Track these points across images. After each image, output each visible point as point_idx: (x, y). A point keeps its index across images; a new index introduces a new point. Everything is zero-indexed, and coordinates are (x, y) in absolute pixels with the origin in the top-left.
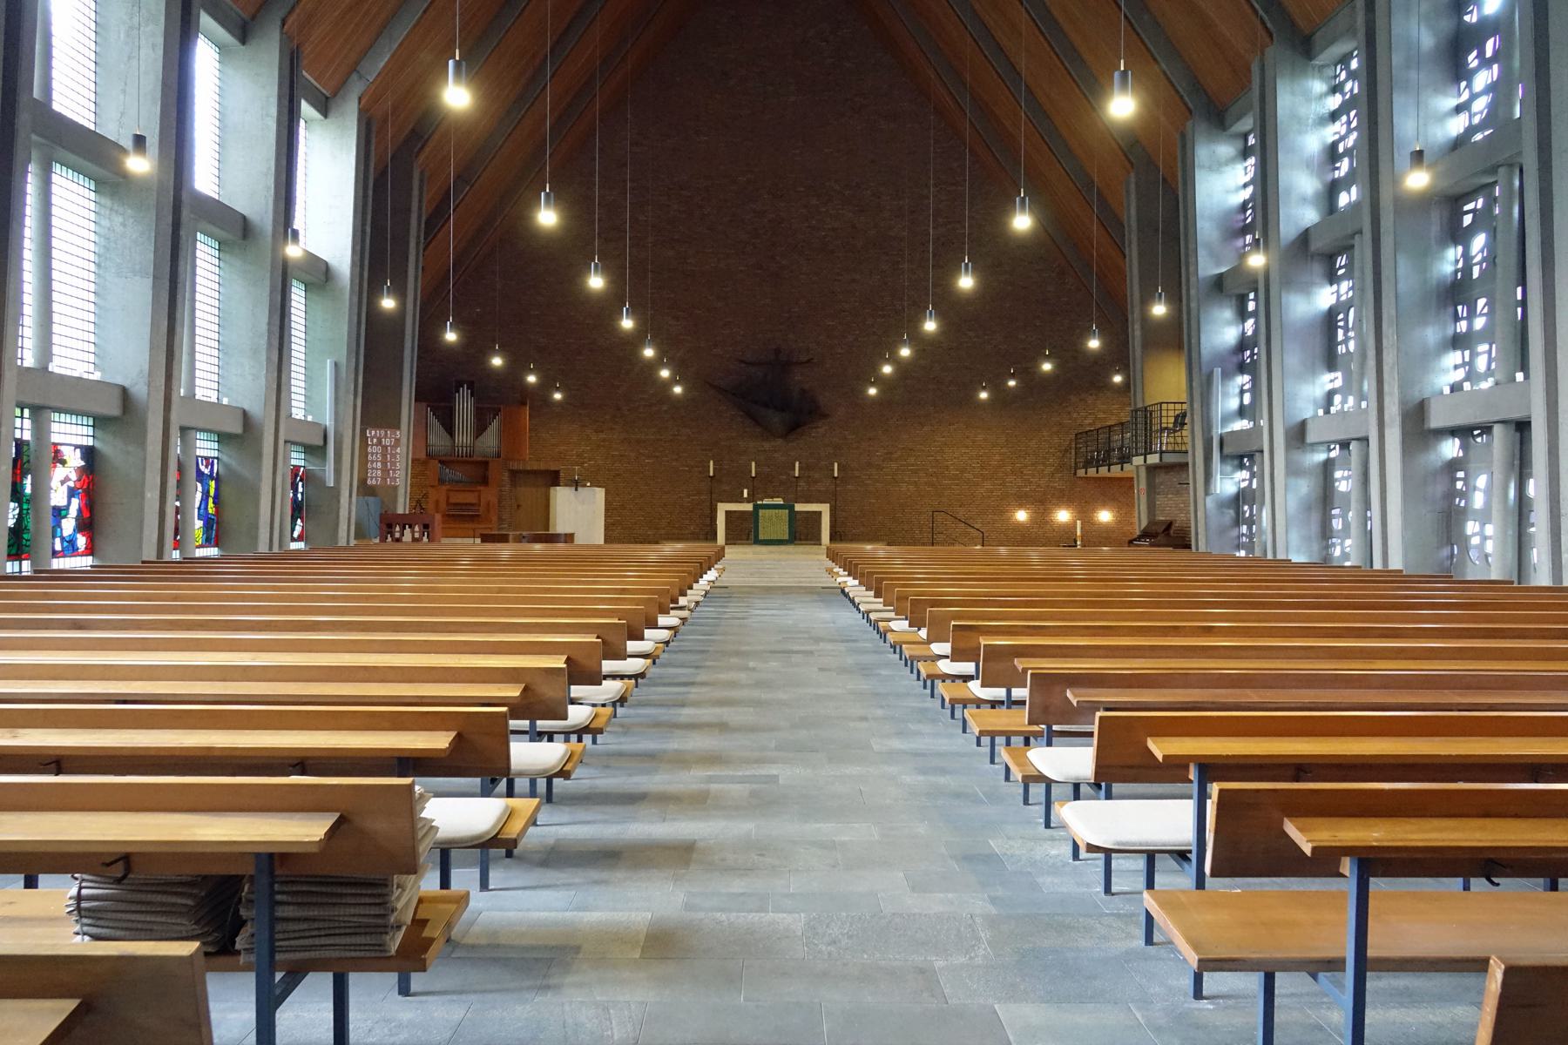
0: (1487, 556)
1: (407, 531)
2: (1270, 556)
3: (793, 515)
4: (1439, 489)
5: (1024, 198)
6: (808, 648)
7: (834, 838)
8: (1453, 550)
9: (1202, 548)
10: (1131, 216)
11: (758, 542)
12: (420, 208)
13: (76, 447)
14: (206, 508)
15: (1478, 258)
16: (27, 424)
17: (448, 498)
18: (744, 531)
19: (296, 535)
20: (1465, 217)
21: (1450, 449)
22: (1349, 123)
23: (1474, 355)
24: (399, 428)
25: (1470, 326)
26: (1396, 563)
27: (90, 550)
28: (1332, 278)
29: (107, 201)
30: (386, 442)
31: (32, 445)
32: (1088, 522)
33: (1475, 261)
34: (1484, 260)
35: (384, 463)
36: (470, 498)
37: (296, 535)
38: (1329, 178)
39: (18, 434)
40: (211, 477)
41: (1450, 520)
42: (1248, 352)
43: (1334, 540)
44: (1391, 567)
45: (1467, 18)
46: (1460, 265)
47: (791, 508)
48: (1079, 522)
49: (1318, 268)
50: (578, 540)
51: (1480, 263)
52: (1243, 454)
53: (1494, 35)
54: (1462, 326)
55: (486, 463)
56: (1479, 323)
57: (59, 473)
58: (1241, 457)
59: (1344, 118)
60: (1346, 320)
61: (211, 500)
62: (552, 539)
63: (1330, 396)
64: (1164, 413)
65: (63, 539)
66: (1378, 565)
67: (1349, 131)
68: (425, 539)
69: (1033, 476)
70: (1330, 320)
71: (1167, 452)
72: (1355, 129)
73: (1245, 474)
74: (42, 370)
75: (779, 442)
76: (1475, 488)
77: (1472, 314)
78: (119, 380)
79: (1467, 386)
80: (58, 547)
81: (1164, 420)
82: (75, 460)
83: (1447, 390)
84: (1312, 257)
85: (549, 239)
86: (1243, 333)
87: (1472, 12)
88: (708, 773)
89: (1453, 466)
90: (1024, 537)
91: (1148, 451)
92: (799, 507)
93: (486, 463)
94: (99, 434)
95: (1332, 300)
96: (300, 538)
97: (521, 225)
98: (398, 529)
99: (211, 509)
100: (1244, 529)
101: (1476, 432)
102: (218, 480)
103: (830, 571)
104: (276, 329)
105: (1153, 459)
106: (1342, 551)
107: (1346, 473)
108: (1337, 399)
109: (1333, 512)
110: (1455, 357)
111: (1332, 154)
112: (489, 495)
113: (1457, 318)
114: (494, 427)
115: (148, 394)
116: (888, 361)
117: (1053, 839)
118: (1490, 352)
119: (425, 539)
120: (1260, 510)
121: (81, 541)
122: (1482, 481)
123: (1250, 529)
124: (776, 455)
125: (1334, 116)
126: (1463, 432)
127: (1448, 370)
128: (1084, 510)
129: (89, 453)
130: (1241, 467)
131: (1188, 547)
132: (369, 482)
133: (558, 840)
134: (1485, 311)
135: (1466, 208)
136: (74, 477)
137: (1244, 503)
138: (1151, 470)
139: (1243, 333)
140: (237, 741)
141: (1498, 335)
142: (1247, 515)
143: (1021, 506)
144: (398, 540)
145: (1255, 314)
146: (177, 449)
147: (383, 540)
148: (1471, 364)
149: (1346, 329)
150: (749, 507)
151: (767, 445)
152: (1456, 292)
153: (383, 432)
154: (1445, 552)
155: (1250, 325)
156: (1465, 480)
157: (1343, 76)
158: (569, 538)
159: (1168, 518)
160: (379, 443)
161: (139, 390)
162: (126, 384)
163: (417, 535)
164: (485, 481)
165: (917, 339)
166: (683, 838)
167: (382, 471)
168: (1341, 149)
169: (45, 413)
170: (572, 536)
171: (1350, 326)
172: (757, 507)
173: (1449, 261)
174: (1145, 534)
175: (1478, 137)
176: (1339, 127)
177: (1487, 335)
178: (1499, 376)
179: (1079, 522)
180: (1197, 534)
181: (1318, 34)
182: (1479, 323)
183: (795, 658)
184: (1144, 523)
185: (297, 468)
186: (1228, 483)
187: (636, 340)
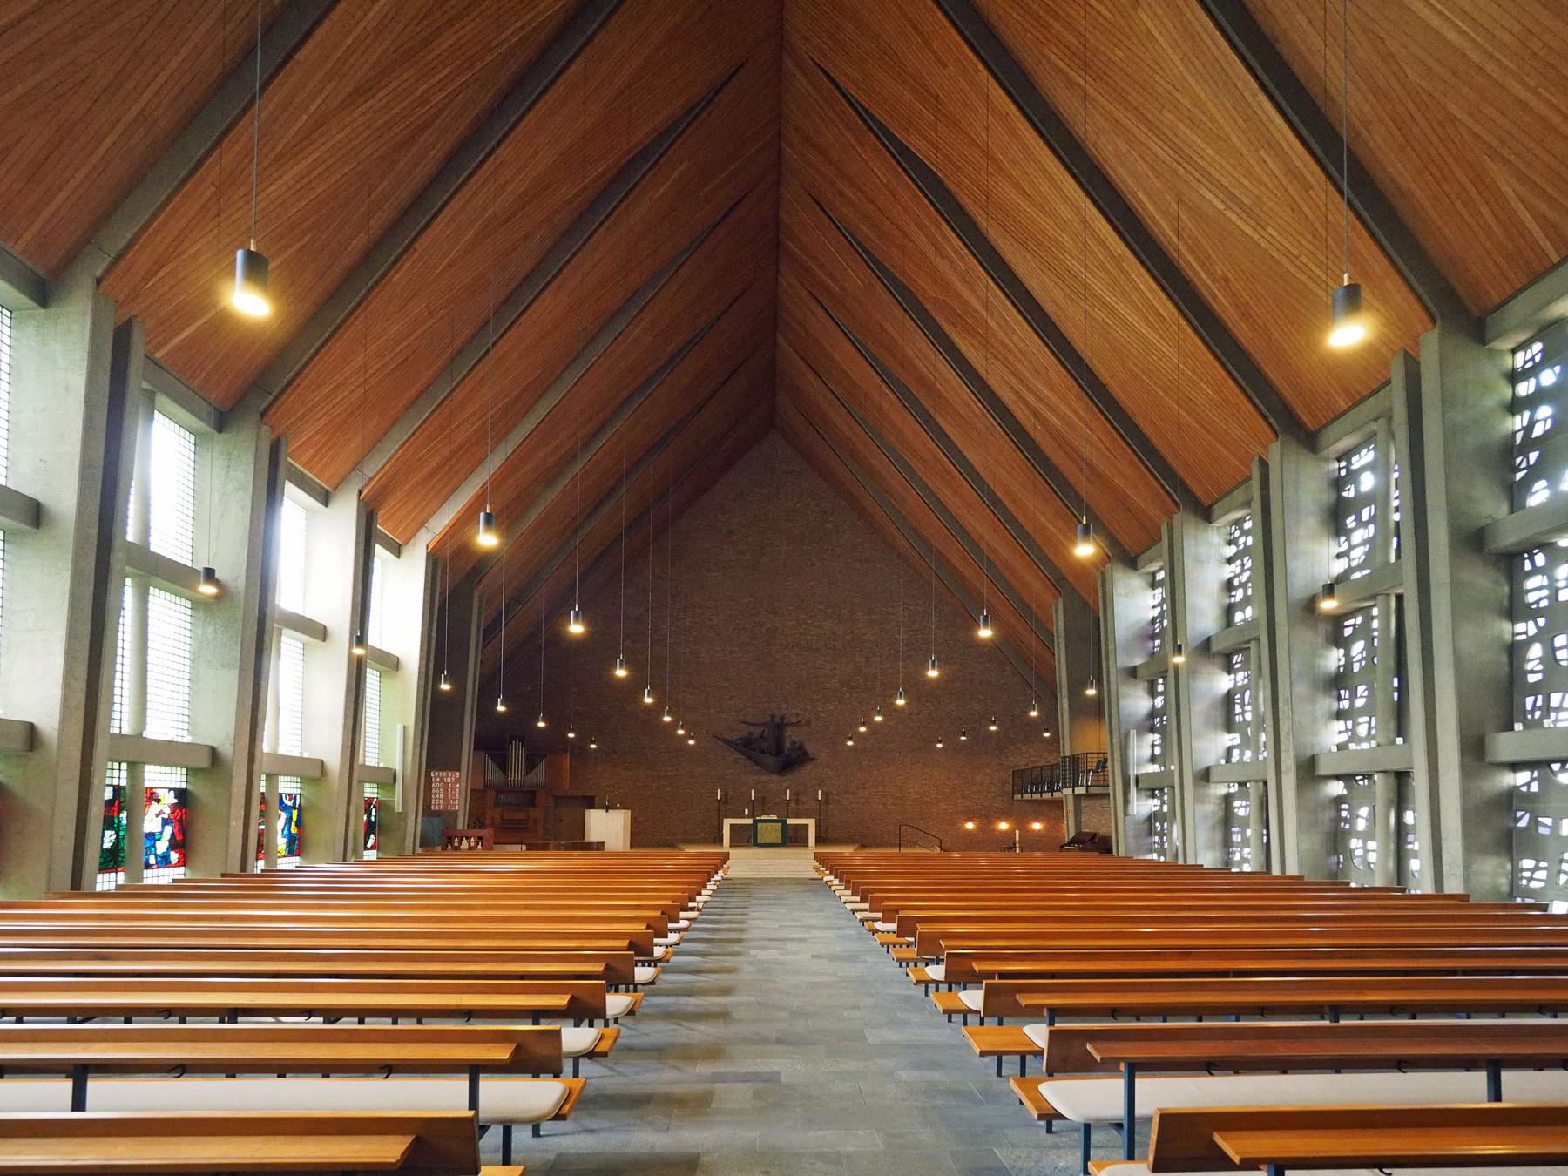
0: (1369, 864)
1: (465, 842)
2: (1181, 862)
3: (785, 826)
4: (1329, 814)
5: (987, 616)
6: (802, 936)
7: (839, 1149)
8: (1339, 858)
9: (1122, 854)
10: (1059, 625)
11: (756, 844)
12: (479, 620)
13: (170, 790)
14: (289, 829)
15: (1359, 657)
16: (124, 774)
17: (502, 816)
18: (745, 838)
19: (369, 845)
20: (1565, 643)
21: (1337, 788)
22: (1243, 565)
23: (1355, 724)
24: (459, 770)
25: (1352, 704)
26: (1292, 870)
27: (183, 862)
28: (1229, 669)
29: (201, 615)
30: (449, 780)
31: (127, 790)
32: (1025, 832)
33: (1355, 660)
34: (1363, 659)
35: (446, 794)
36: (522, 816)
37: (369, 845)
38: (1227, 601)
39: (116, 782)
40: (294, 807)
41: (1337, 839)
42: (1158, 719)
43: (1234, 849)
44: (1288, 873)
45: (1345, 494)
46: (1342, 662)
47: (784, 822)
48: (1017, 832)
49: (1219, 661)
50: (608, 847)
51: (1360, 661)
52: (1152, 788)
53: (1370, 505)
54: (1345, 705)
55: (534, 792)
56: (1360, 703)
57: (154, 808)
58: (1153, 790)
59: (1239, 562)
60: (1243, 698)
61: (293, 824)
62: (589, 847)
63: (1229, 750)
64: (1089, 760)
65: (156, 856)
66: (1276, 871)
67: (1243, 570)
68: (479, 847)
69: (979, 799)
70: (1229, 699)
71: (1091, 786)
72: (1248, 569)
73: (1157, 802)
74: (139, 736)
75: (775, 777)
76: (1358, 816)
77: (1353, 696)
78: (210, 742)
79: (1352, 746)
80: (152, 860)
81: (1090, 764)
82: (169, 799)
83: (1335, 749)
84: (1213, 656)
85: (579, 643)
86: (1154, 706)
87: (1349, 490)
88: (714, 1070)
89: (1338, 801)
90: (971, 843)
91: (1075, 785)
92: (790, 821)
93: (534, 792)
94: (190, 779)
95: (1231, 685)
96: (373, 848)
97: (557, 637)
98: (456, 840)
99: (294, 829)
100: (1156, 839)
101: (1358, 778)
102: (300, 809)
103: (817, 869)
104: (352, 705)
105: (1081, 791)
106: (1242, 856)
107: (1244, 803)
108: (1236, 752)
109: (1233, 829)
110: (1340, 725)
111: (1229, 586)
112: (536, 813)
113: (1340, 699)
114: (541, 767)
115: (234, 753)
116: (863, 724)
117: (1057, 1147)
118: (1369, 723)
119: (479, 847)
120: (1171, 826)
121: (174, 856)
122: (1364, 811)
123: (1161, 838)
124: (771, 785)
125: (1230, 561)
126: (1347, 778)
127: (1333, 734)
128: (1021, 821)
129: (180, 794)
130: (1154, 796)
131: (1109, 851)
132: (433, 808)
133: (559, 1155)
134: (1366, 693)
135: (1346, 623)
136: (168, 811)
137: (1156, 821)
138: (1077, 798)
139: (1154, 706)
140: (146, 1155)
141: (1379, 710)
142: (1159, 829)
143: (969, 820)
144: (457, 849)
145: (1163, 693)
146: (262, 786)
147: (444, 849)
148: (1353, 730)
149: (1243, 705)
150: (750, 821)
151: (764, 778)
152: (1339, 681)
153: (445, 774)
154: (1334, 859)
155: (1159, 702)
156: (1349, 811)
157: (1237, 533)
158: (600, 846)
159: (1092, 831)
160: (443, 781)
161: (226, 749)
162: (215, 745)
163: (472, 844)
164: (533, 804)
165: (889, 711)
166: (685, 1151)
167: (444, 800)
168: (1236, 582)
169: (139, 766)
170: (603, 844)
171: (1246, 702)
172: (755, 822)
173: (1334, 659)
174: (1072, 842)
175: (1356, 576)
176: (1235, 568)
177: (1368, 710)
178: (1381, 740)
179: (1017, 832)
180: (1117, 842)
181: (1216, 506)
182: (1360, 703)
183: (790, 946)
184: (1072, 834)
185: (371, 799)
186: (1142, 806)
187: (657, 709)
